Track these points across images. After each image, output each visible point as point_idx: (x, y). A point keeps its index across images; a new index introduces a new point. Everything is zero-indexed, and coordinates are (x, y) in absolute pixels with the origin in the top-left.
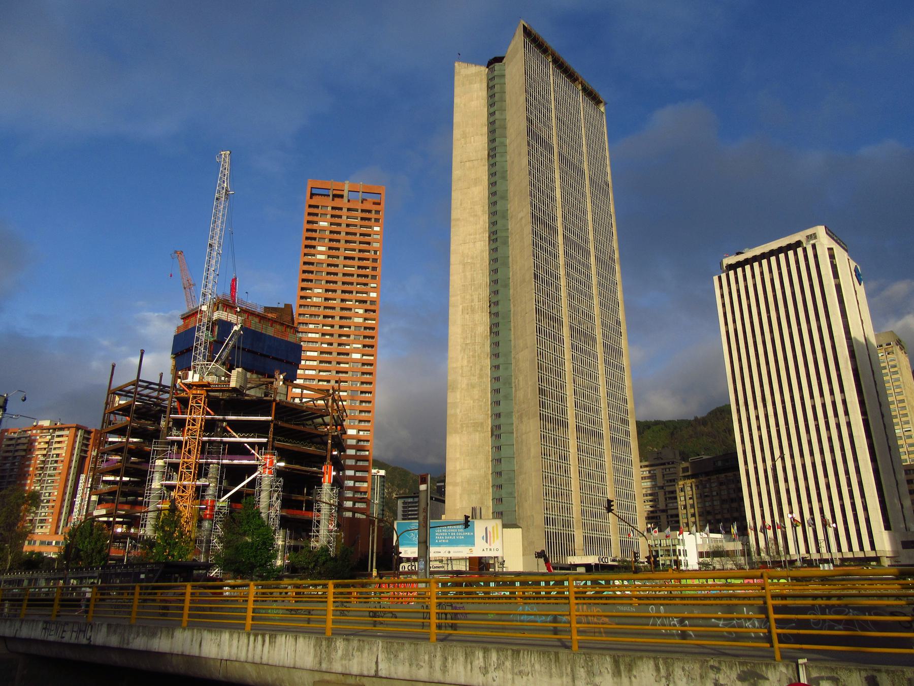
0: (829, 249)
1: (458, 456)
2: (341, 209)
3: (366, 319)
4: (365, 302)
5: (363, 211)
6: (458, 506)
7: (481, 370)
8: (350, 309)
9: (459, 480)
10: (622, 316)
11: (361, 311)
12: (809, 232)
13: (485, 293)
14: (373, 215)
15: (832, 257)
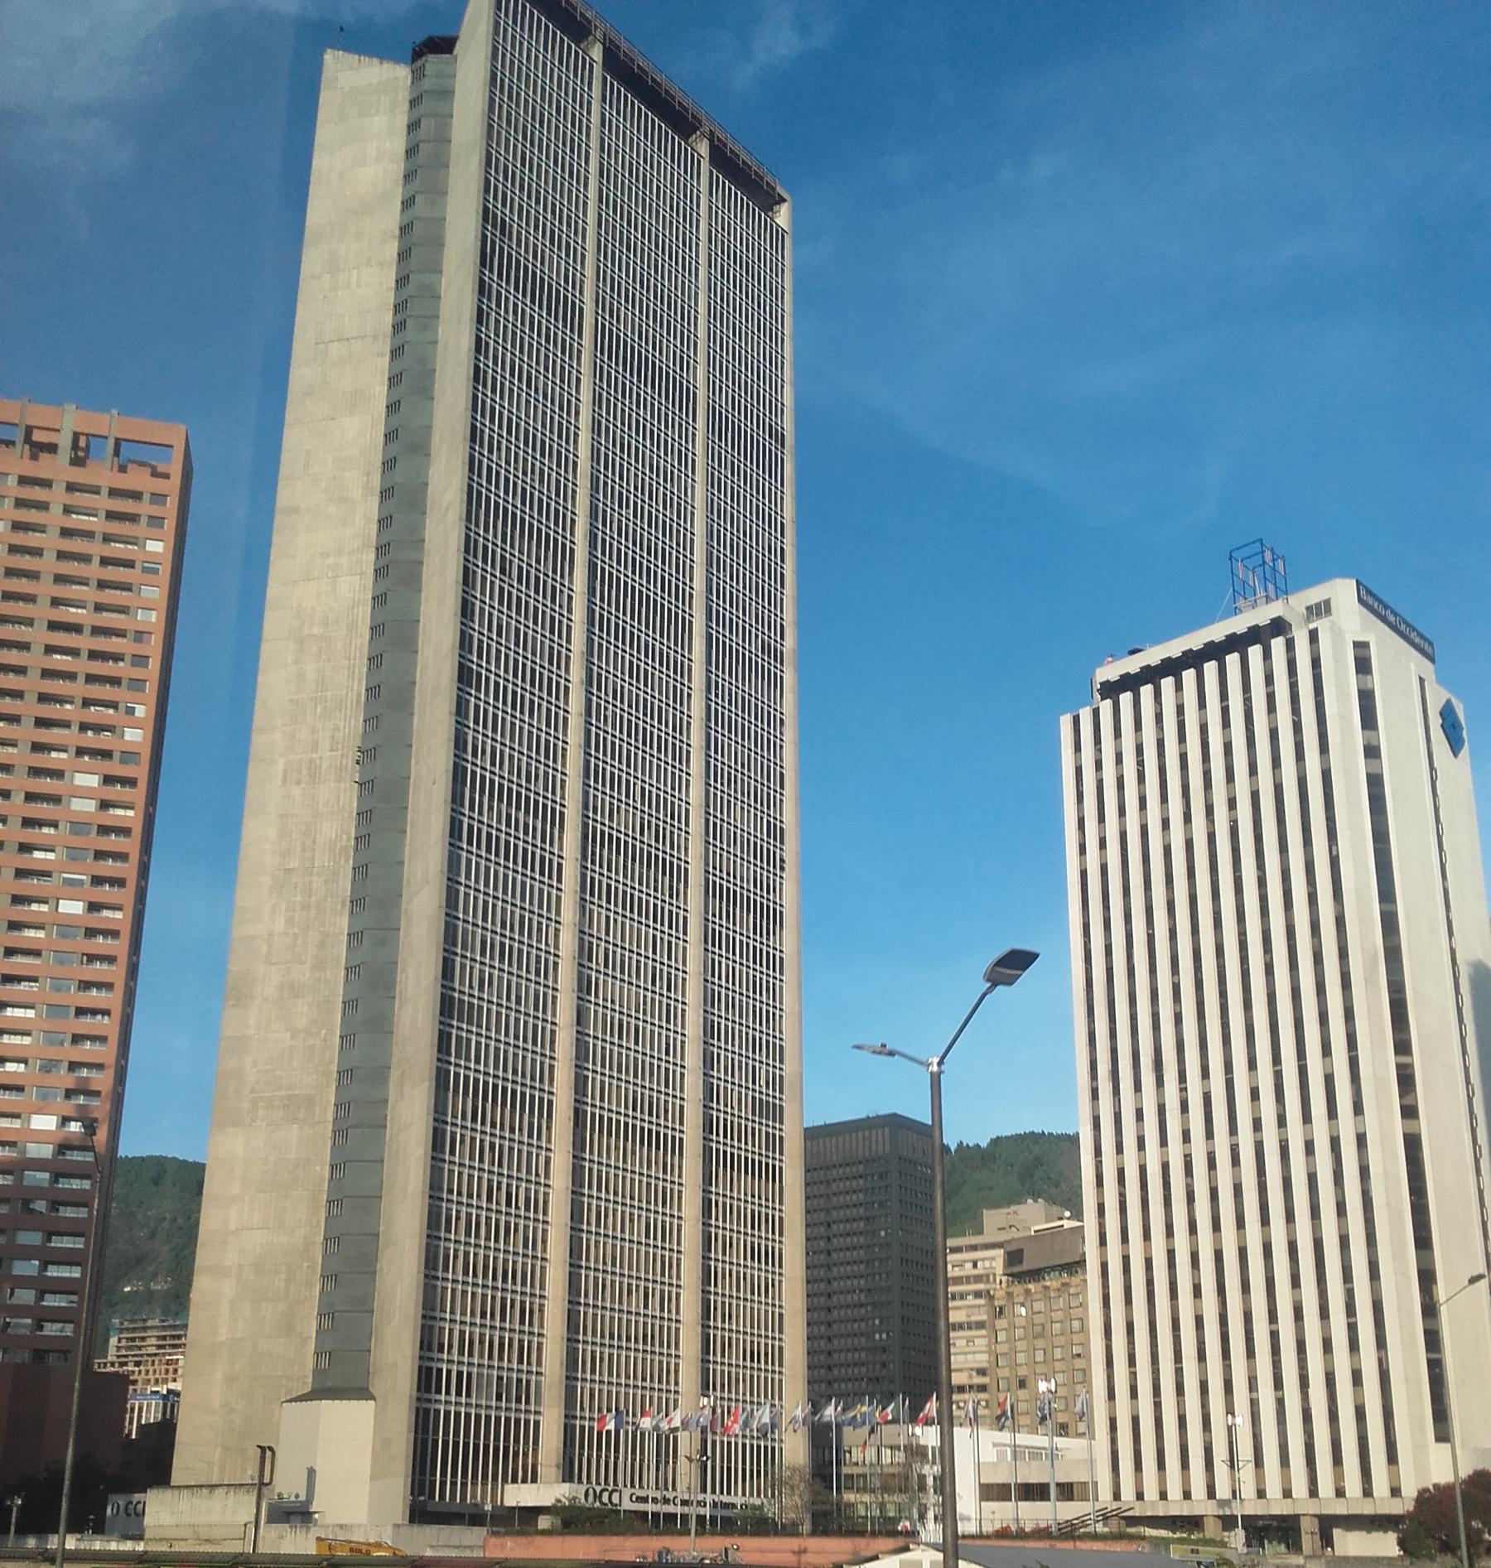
0: (1356, 645)
1: (236, 1190)
2: (46, 484)
3: (105, 805)
4: (106, 754)
5: (114, 493)
6: (224, 1334)
7: (322, 945)
8: (58, 774)
9: (231, 1258)
10: (789, 817)
11: (93, 781)
12: (1314, 595)
13: (350, 725)
14: (144, 508)
15: (1363, 666)
